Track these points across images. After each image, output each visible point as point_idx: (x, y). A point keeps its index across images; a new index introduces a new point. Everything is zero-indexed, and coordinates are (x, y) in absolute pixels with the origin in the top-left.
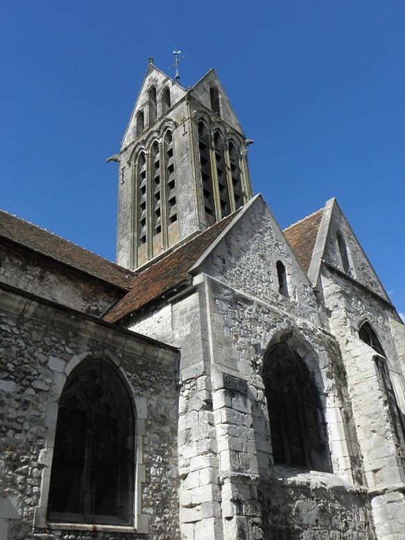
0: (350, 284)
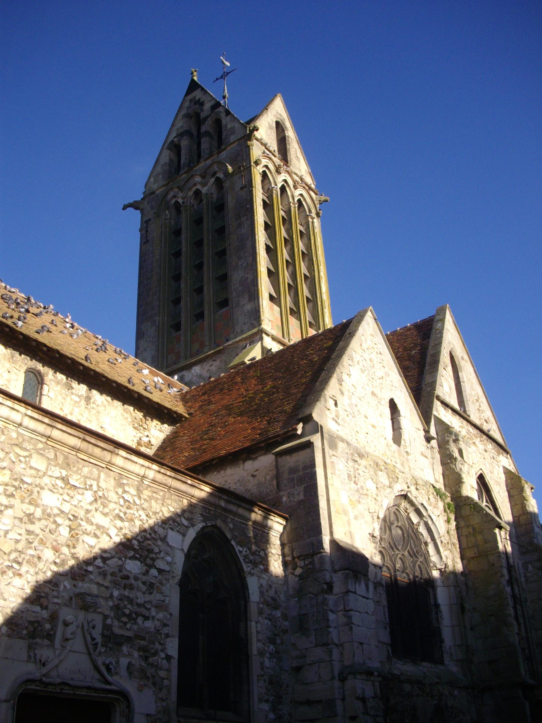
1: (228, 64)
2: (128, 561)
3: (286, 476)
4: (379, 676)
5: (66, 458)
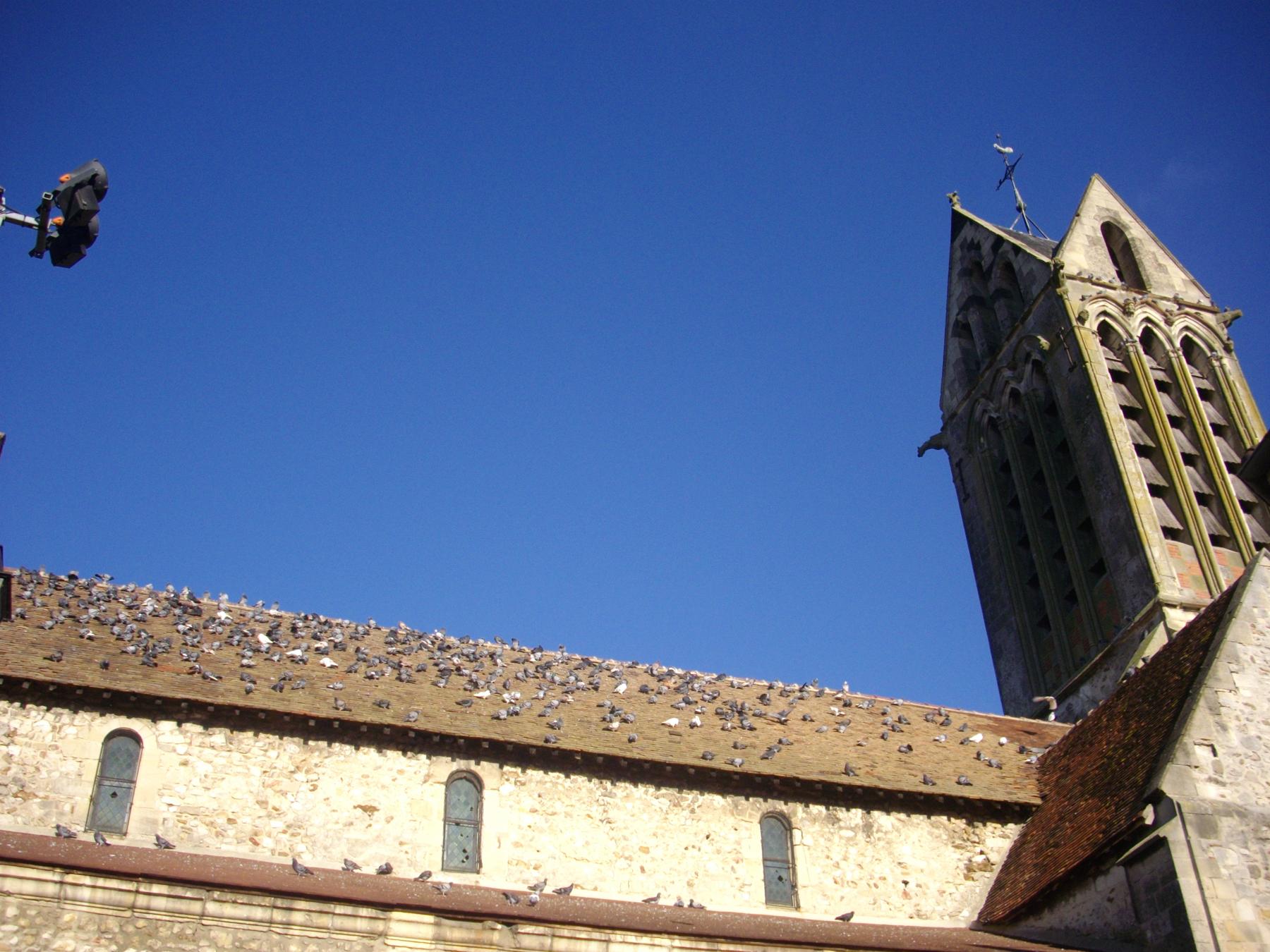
1: (1009, 150)
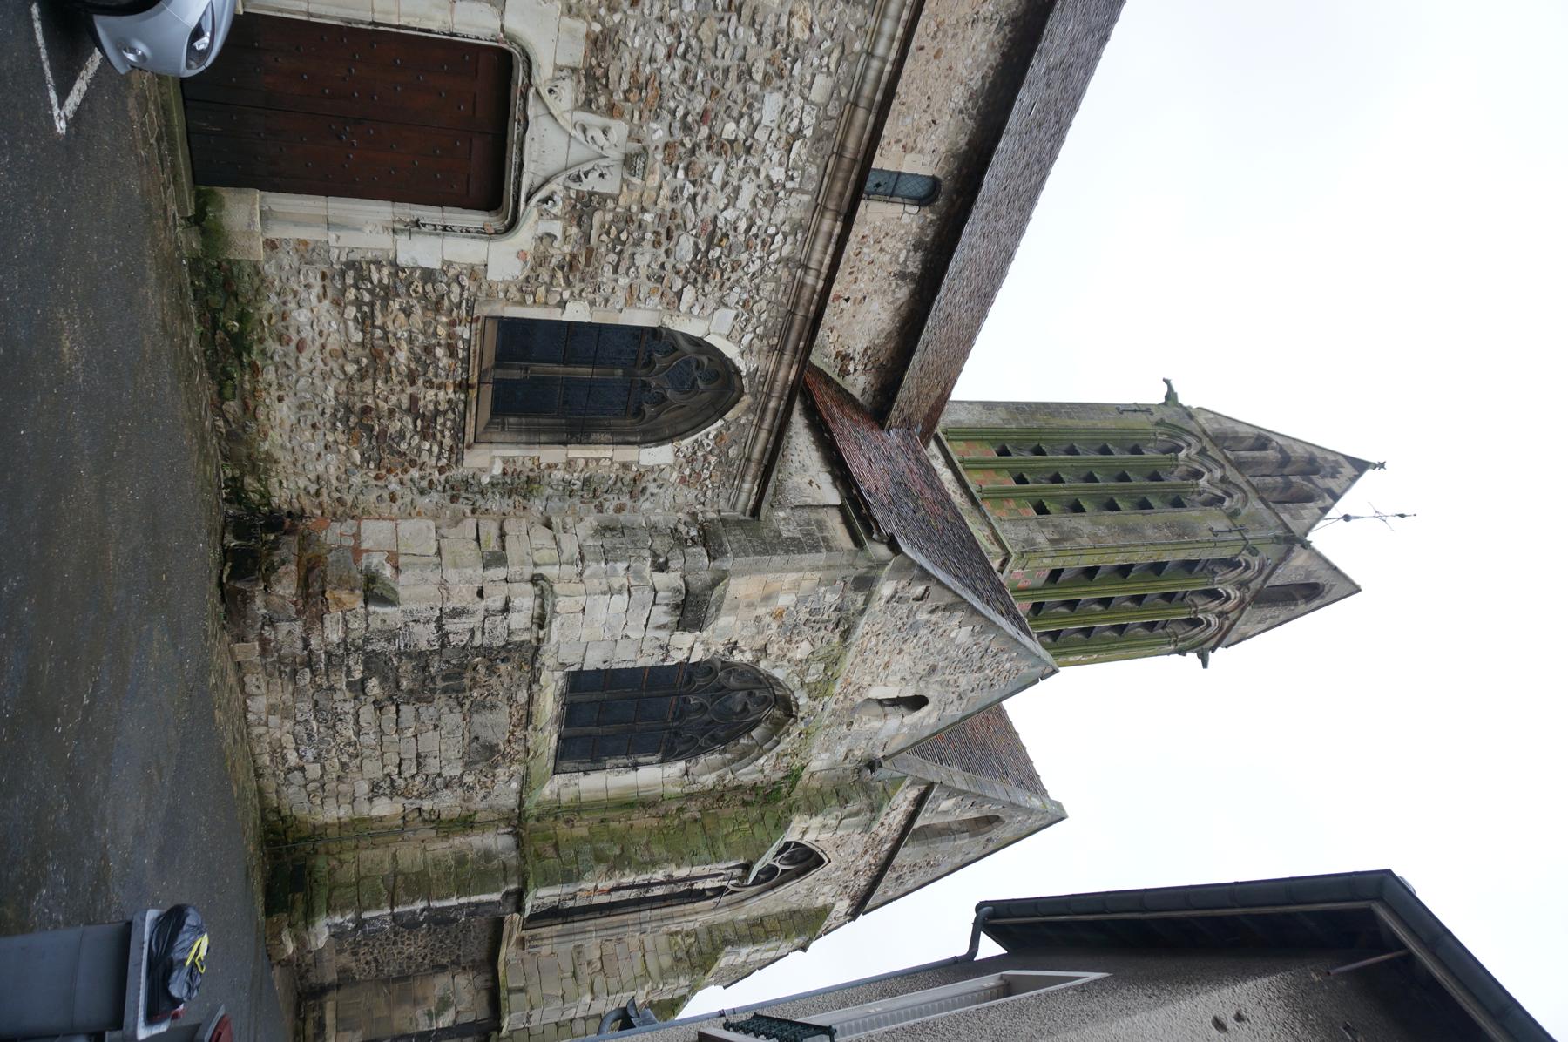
0: (896, 835)
2: (692, 239)
3: (814, 516)
4: (539, 640)
5: (829, 136)
